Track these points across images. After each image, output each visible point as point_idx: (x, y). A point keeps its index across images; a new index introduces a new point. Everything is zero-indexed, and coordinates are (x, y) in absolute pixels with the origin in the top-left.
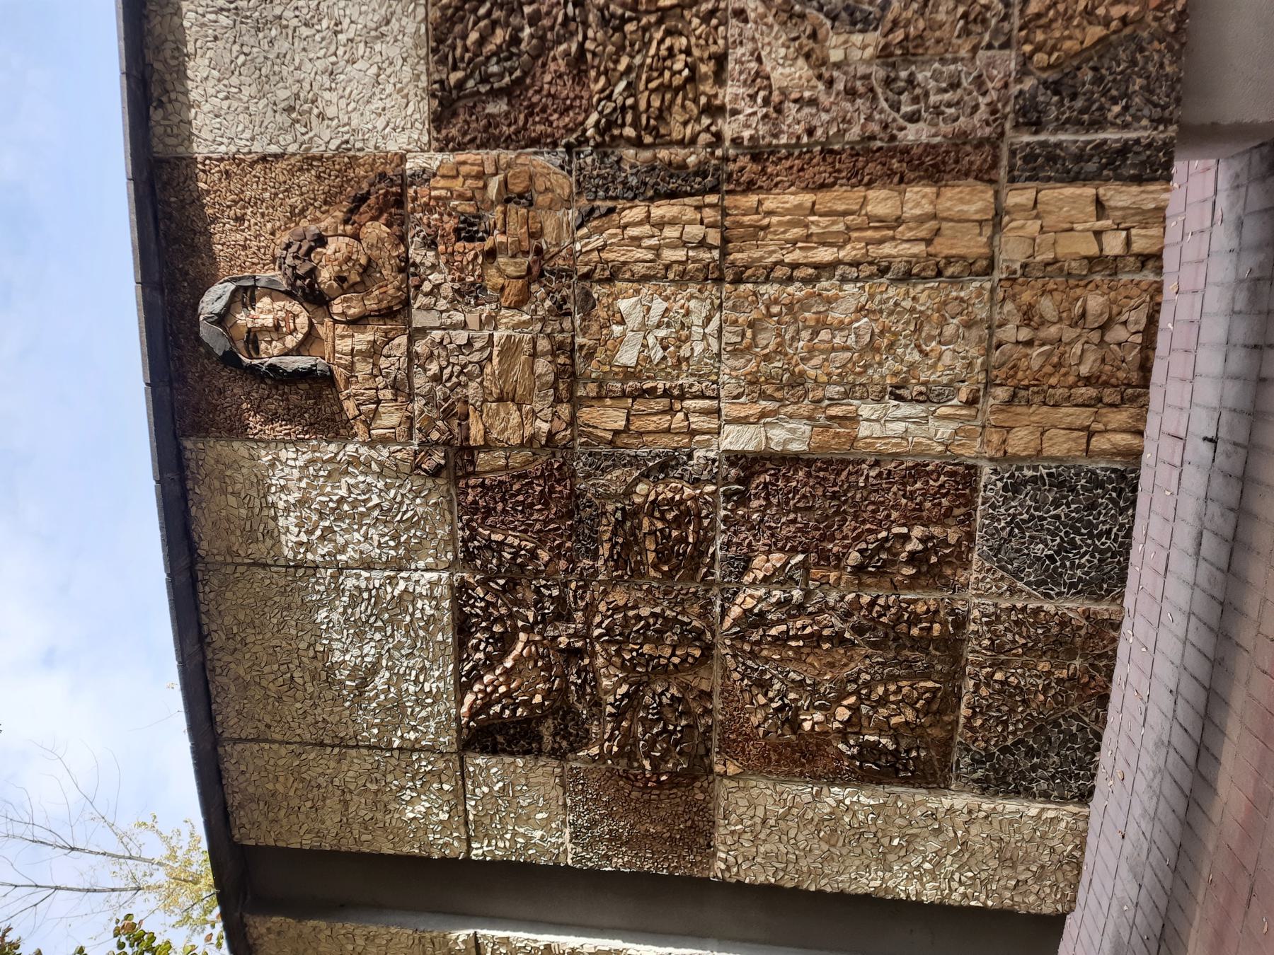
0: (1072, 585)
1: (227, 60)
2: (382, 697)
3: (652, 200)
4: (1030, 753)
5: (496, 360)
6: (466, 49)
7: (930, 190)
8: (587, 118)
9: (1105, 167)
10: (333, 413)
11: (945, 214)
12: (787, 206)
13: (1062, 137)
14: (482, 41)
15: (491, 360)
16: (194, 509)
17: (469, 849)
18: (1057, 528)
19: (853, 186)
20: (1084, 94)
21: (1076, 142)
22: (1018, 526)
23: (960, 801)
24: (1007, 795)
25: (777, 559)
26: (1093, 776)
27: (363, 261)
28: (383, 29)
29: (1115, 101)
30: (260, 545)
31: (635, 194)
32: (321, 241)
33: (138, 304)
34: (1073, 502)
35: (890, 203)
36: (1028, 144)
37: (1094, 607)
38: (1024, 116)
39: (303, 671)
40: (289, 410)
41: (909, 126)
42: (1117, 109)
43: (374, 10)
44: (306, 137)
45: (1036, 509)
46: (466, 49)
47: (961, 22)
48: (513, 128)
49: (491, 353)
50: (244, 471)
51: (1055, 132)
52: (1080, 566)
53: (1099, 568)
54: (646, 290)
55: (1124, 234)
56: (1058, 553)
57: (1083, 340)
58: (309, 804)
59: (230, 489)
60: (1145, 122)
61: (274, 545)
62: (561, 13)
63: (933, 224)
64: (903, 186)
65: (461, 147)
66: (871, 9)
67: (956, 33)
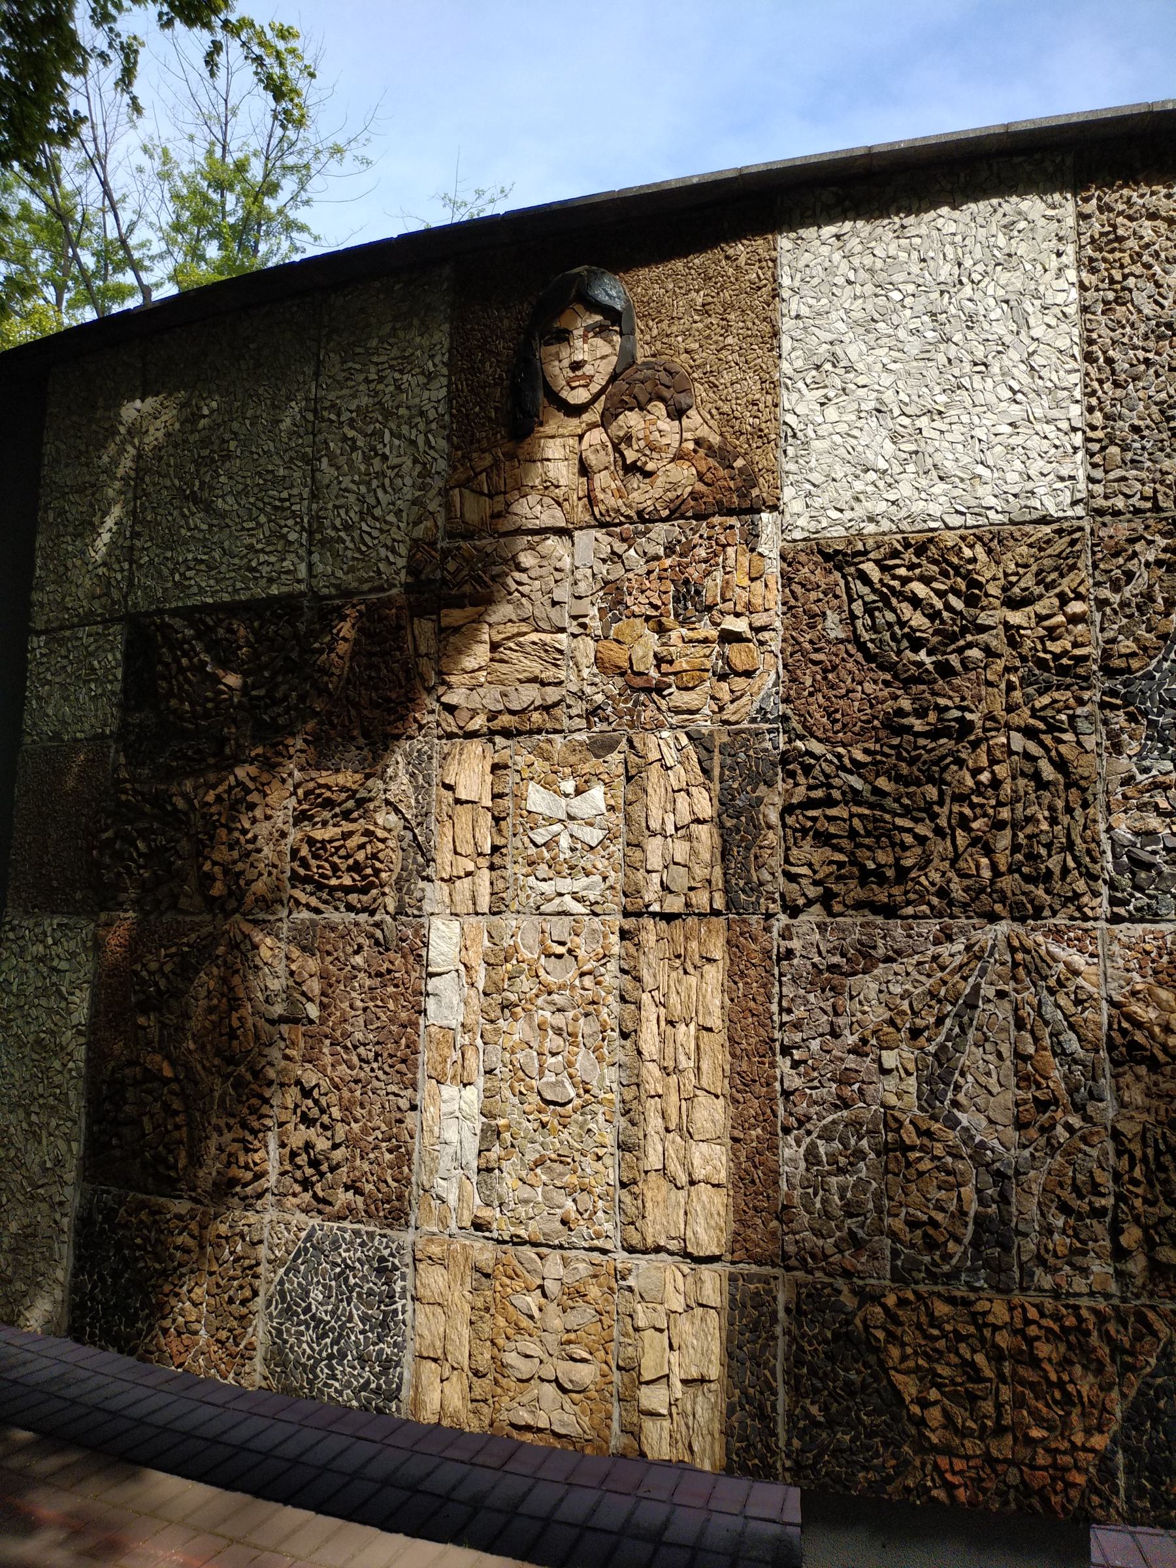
0: (279, 1333)
1: (895, 278)
2: (183, 523)
3: (721, 826)
4: (117, 1275)
5: (535, 637)
6: (905, 581)
7: (722, 1177)
8: (820, 740)
9: (744, 1393)
10: (479, 441)
11: (693, 1194)
12: (709, 997)
13: (782, 1342)
14: (915, 602)
15: (536, 630)
16: (377, 284)
17: (38, 634)
18: (339, 1319)
19: (731, 1078)
20: (833, 1370)
21: (775, 1358)
22: (342, 1272)
23: (71, 1196)
24: (77, 1246)
25: (314, 986)
26: (94, 1343)
27: (650, 466)
28: (934, 473)
29: (825, 1409)
30: (338, 366)
31: (725, 803)
32: (677, 413)
33: (641, 187)
34: (366, 1338)
35: (709, 1125)
36: (775, 1299)
37: (259, 1355)
38: (809, 1295)
39: (210, 428)
40: (484, 388)
41: (802, 1150)
42: (814, 1410)
43: (957, 460)
44: (800, 385)
45: (359, 1295)
46: (905, 581)
47: (925, 1218)
48: (807, 646)
49: (544, 631)
50: (418, 339)
51: (787, 1332)
52: (300, 1342)
53: (297, 1362)
54: (617, 819)
55: (665, 1412)
56: (313, 1317)
57: (545, 1357)
58: (83, 448)
59: (398, 325)
60: (796, 1443)
61: (338, 382)
62: (950, 704)
63: (683, 1179)
64: (729, 1142)
65: (787, 580)
66: (947, 1102)
67: (911, 1211)
